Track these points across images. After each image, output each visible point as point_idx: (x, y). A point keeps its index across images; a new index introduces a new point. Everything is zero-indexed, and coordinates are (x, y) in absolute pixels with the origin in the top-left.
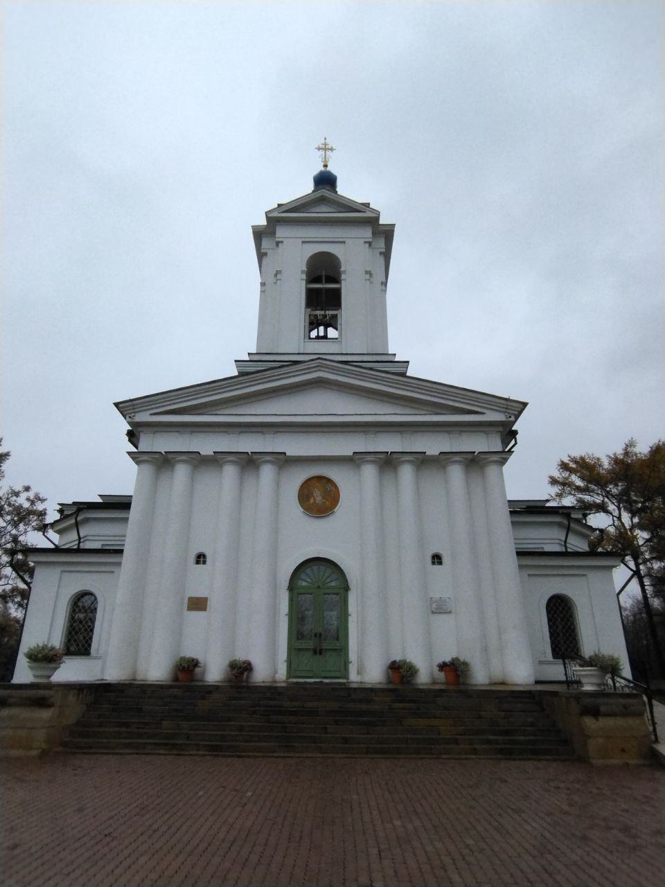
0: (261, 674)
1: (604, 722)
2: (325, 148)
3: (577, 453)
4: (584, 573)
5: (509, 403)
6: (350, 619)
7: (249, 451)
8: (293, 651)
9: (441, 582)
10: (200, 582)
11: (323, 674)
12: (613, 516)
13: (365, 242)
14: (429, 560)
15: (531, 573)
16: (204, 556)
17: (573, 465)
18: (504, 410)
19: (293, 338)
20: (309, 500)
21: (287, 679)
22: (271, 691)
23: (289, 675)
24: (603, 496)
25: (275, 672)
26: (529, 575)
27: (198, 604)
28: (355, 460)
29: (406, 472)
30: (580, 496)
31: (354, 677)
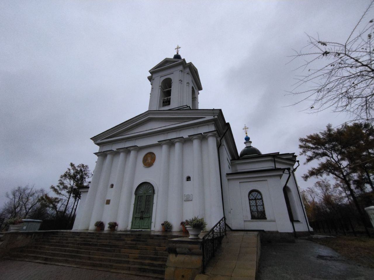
0: (121, 227)
1: (180, 258)
2: (178, 48)
3: (309, 135)
4: (266, 179)
5: (214, 111)
6: (154, 205)
8: (134, 218)
9: (190, 188)
10: (111, 194)
11: (143, 227)
12: (330, 157)
13: (180, 71)
15: (240, 181)
17: (309, 139)
18: (213, 114)
21: (131, 229)
22: (125, 234)
23: (132, 228)
24: (323, 149)
25: (128, 227)
26: (240, 182)
28: (159, 145)
29: (177, 146)
30: (314, 151)
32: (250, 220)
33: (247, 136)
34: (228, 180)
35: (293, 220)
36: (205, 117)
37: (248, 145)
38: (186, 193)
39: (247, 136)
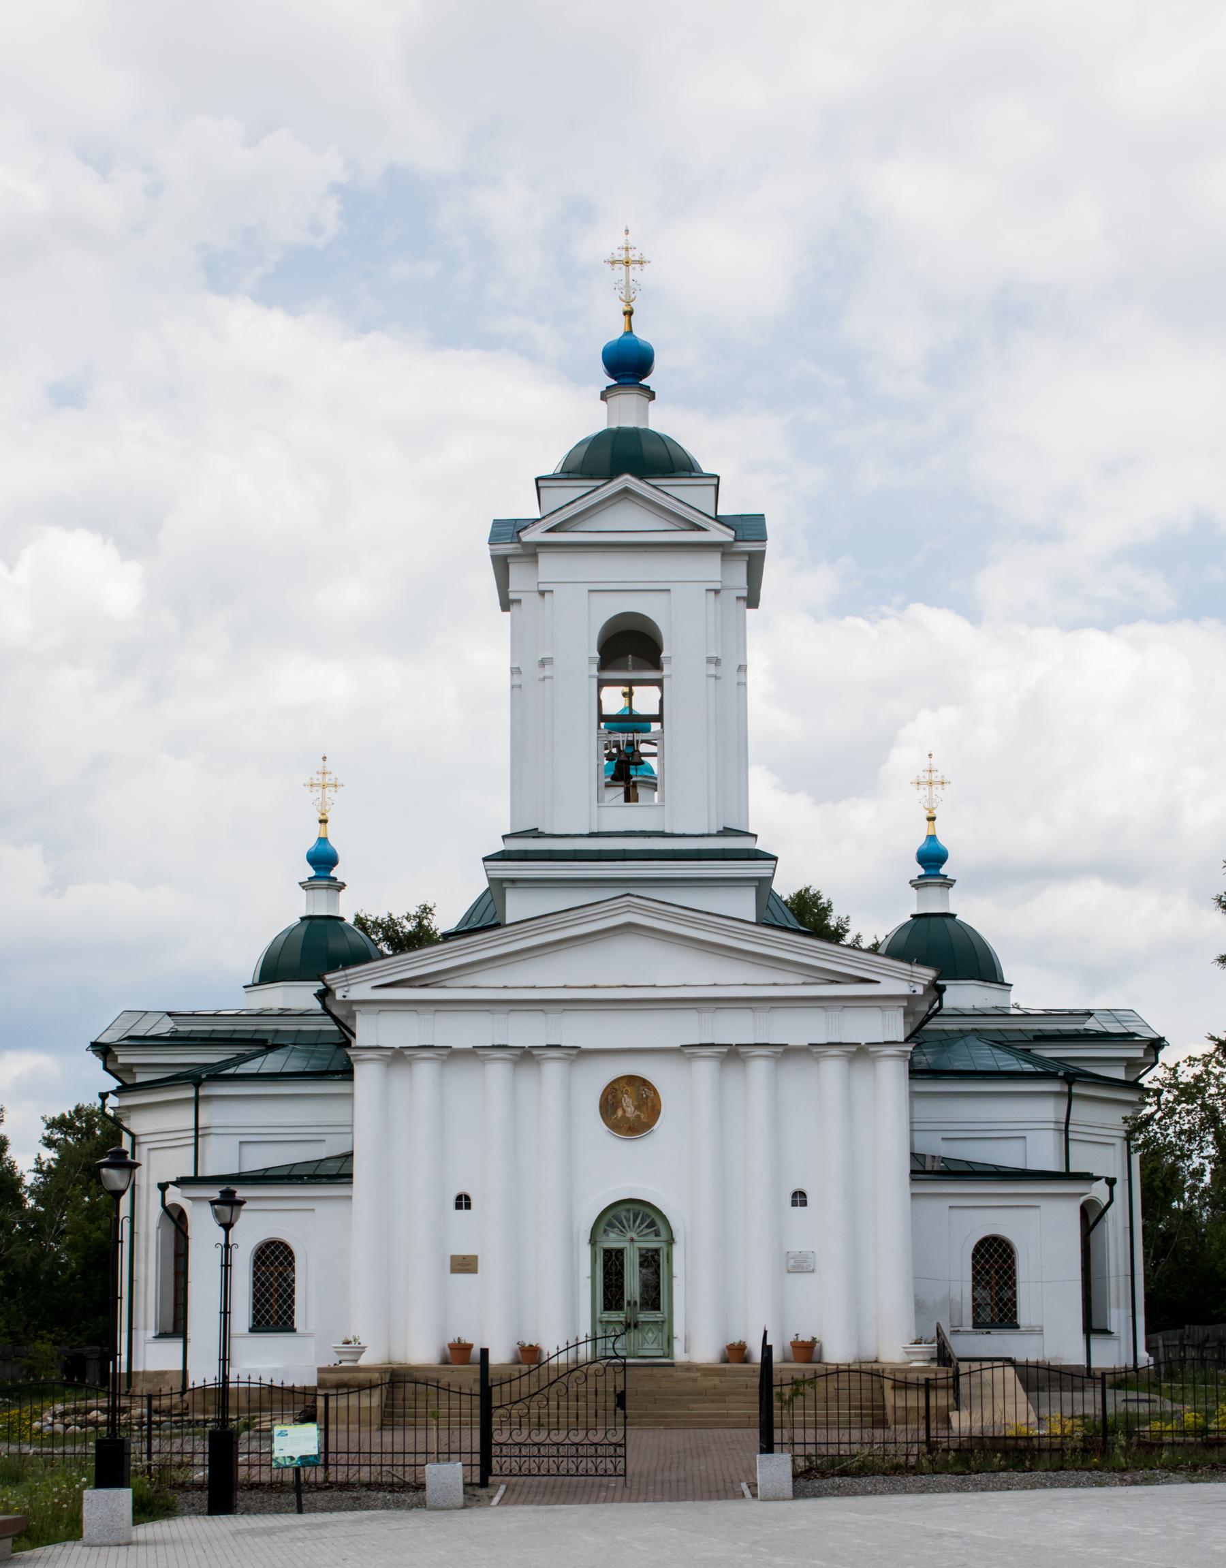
7: (527, 1045)
10: (465, 1234)
14: (789, 1200)
16: (467, 1198)
19: (581, 805)
20: (615, 1112)
27: (464, 1265)
28: (685, 1052)
31: (679, 1356)
32: (970, 1329)
33: (932, 838)
34: (913, 1195)
35: (1093, 1327)
36: (549, 531)
37: (933, 903)
38: (795, 1247)
39: (932, 838)
